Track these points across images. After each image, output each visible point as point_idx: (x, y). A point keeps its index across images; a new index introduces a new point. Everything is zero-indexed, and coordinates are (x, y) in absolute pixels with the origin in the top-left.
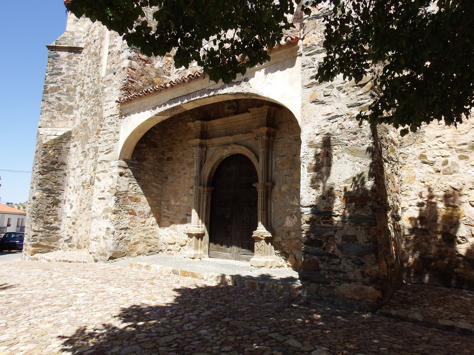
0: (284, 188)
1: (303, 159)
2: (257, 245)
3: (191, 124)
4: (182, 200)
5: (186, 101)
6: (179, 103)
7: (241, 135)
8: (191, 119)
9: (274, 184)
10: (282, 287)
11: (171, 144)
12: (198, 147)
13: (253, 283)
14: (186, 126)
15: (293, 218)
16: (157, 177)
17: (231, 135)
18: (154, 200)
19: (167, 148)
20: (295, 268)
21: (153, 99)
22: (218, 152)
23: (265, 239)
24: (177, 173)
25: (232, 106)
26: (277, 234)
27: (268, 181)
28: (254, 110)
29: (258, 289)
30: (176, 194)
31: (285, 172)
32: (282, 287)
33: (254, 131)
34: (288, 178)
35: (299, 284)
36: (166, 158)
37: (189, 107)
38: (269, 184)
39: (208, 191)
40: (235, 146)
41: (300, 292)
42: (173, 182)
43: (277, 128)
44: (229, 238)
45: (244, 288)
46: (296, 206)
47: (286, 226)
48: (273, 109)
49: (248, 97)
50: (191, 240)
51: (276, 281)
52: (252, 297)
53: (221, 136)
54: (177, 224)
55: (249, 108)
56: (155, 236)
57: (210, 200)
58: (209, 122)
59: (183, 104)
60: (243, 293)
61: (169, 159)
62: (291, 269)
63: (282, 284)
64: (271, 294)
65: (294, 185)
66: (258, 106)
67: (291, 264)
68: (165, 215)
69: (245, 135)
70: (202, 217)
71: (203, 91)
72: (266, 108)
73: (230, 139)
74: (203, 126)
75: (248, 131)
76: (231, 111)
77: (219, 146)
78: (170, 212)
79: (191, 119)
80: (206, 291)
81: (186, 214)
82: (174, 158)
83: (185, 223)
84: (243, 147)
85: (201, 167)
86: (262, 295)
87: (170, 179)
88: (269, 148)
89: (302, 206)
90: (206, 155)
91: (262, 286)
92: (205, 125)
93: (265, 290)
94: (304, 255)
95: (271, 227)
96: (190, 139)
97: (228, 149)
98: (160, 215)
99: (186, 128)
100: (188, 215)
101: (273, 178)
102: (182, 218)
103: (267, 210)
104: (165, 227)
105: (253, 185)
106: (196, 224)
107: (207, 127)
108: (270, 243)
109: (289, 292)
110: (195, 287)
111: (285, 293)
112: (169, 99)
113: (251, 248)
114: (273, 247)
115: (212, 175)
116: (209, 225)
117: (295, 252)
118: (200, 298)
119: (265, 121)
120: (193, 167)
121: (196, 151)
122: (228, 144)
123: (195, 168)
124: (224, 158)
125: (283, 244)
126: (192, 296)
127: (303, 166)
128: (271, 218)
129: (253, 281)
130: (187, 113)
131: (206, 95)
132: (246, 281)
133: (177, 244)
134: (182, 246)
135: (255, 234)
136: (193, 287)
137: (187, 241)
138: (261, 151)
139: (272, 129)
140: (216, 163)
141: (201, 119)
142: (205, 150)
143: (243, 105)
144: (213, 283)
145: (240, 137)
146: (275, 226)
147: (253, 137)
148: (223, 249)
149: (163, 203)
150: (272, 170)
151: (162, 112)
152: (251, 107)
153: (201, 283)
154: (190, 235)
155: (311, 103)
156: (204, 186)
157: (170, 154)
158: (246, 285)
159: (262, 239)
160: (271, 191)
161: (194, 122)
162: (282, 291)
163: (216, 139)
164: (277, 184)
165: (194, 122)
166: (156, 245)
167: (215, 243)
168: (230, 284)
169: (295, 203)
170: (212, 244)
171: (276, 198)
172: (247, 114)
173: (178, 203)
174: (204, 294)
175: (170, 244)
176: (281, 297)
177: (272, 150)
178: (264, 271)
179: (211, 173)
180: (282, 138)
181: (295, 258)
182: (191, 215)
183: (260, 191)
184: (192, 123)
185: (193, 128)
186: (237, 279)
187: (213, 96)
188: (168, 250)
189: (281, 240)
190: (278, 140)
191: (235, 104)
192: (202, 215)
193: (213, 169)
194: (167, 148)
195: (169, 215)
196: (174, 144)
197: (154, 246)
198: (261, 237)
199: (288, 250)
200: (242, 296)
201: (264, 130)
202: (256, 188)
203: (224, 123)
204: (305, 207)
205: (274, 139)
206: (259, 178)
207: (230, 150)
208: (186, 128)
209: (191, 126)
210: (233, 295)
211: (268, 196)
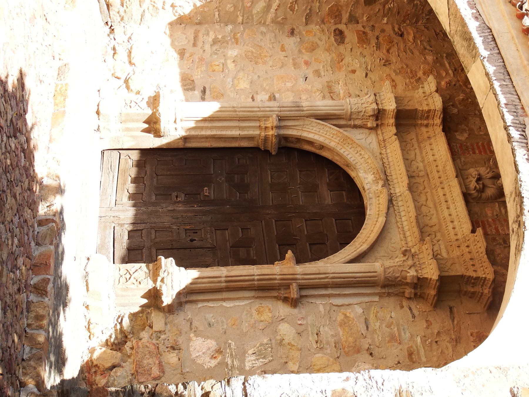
0: (286, 330)
1: (366, 376)
2: (140, 269)
3: (430, 84)
4: (241, 75)
5: (491, 69)
6: (484, 52)
7: (413, 214)
8: (443, 83)
9: (294, 303)
10: (41, 339)
11: (377, 38)
12: (374, 106)
13: (47, 266)
14: (426, 74)
15: (213, 357)
16: (292, 9)
17: (411, 188)
18: (235, 7)
19: (367, 30)
20: (89, 369)
22: (365, 157)
23: (155, 288)
24: (306, 58)
25: (484, 186)
26: (171, 317)
27: (302, 288)
28: (479, 242)
29: (35, 280)
30: (254, 58)
31: (327, 332)
32: (41, 339)
33: (424, 247)
34: (312, 338)
35: (51, 380)
36: (342, 27)
37: (476, 78)
38: (294, 293)
39: (266, 139)
40: (384, 200)
41: (31, 385)
42: (283, 49)
43: (438, 303)
44: (154, 197)
45: (33, 244)
46: (243, 362)
47: (190, 340)
48: (486, 291)
49: (513, 226)
50: (144, 104)
51: (55, 325)
52: (15, 267)
53: (408, 162)
54: (180, 66)
55: (484, 229)
56: (147, 15)
57: (245, 144)
58: (439, 130)
59: (482, 61)
60: (21, 244)
61: (340, 35)
62: (86, 359)
63: (48, 339)
64: (22, 313)
65: (296, 354)
66: (490, 253)
67: (98, 358)
68: (200, 35)
69: (414, 224)
70: (202, 128)
71: (520, 111)
72: (487, 272)
73: (400, 186)
74: (428, 114)
75: (424, 231)
76: (473, 184)
77: (382, 159)
78: (207, 47)
79: (443, 83)
80: (23, 151)
81: (205, 89)
82: (342, 48)
83: (183, 85)
84: (382, 220)
85: (325, 118)
86: (19, 290)
87: (291, 42)
88: (384, 286)
89: (246, 380)
90: (355, 127)
91: (40, 290)
92: (431, 122)
93: (33, 297)
94: (124, 393)
95: (187, 302)
96: (394, 86)
97: (376, 181)
98: (200, 23)
99: (420, 74)
100: (204, 91)
101: (310, 300)
102: (194, 78)
103: (228, 289)
104: (171, 36)
105: (290, 252)
106: (182, 118)
107: (427, 126)
108: (145, 301)
109: (30, 359)
110: (30, 124)
111: (27, 349)
112: (491, 26)
113: (132, 254)
114: (137, 309)
115: (307, 147)
116: (181, 145)
117: (128, 367)
118: (5, 138)
119: (453, 273)
120: (324, 97)
121: (366, 104)
122: (387, 182)
123: (324, 105)
124: (353, 174)
125: (145, 335)
126: (9, 117)
127: (347, 379)
128: (208, 301)
129: (52, 265)
130: (460, 71)
131: (509, 118)
132: (52, 247)
133: (129, 69)
134: (126, 81)
135: (168, 264)
136: (29, 118)
137: (138, 93)
138: (376, 267)
139: (433, 292)
140: (338, 154)
141: (445, 110)
142: (369, 125)
143: (489, 213)
144: (43, 167)
145: (406, 209)
146: (190, 311)
147: (410, 244)
148: (125, 184)
149: (230, 27)
150: (329, 296)
151: (457, 11)
152: (486, 234)
153: (39, 137)
154: (154, 101)
155: (511, 391)
156: (278, 127)
157: (351, 36)
158: (42, 249)
159: (155, 281)
160: (277, 298)
161: (437, 91)
162: (32, 340)
163: (399, 152)
164: (295, 311)
165: (437, 91)
166: (126, 19)
167: (140, 165)
168: (42, 209)
169: (250, 362)
170: (135, 156)
171: (259, 312)
172: (467, 226)
173: (231, 65)
174: (16, 148)
176: (16, 339)
177: (381, 295)
178: (76, 294)
179: (310, 143)
180: (414, 317)
181: (114, 367)
182: (203, 99)
183: (276, 270)
184: (434, 88)
185: (421, 90)
186: (55, 226)
187: (509, 136)
188: (114, 49)
189: (156, 328)
190: (406, 308)
191: (490, 192)
192: (207, 128)
193: (322, 147)
194: (367, 30)
195: (200, 44)
196: (378, 46)
197: (122, 13)
198: (159, 279)
199: (132, 348)
200: (16, 241)
201: (431, 272)
202: (283, 258)
203: (440, 168)
204: (245, 389)
205: (409, 299)
206: (307, 265)
207: (374, 188)
208: (420, 74)
209: (426, 85)
210: (16, 220)
211: (264, 289)
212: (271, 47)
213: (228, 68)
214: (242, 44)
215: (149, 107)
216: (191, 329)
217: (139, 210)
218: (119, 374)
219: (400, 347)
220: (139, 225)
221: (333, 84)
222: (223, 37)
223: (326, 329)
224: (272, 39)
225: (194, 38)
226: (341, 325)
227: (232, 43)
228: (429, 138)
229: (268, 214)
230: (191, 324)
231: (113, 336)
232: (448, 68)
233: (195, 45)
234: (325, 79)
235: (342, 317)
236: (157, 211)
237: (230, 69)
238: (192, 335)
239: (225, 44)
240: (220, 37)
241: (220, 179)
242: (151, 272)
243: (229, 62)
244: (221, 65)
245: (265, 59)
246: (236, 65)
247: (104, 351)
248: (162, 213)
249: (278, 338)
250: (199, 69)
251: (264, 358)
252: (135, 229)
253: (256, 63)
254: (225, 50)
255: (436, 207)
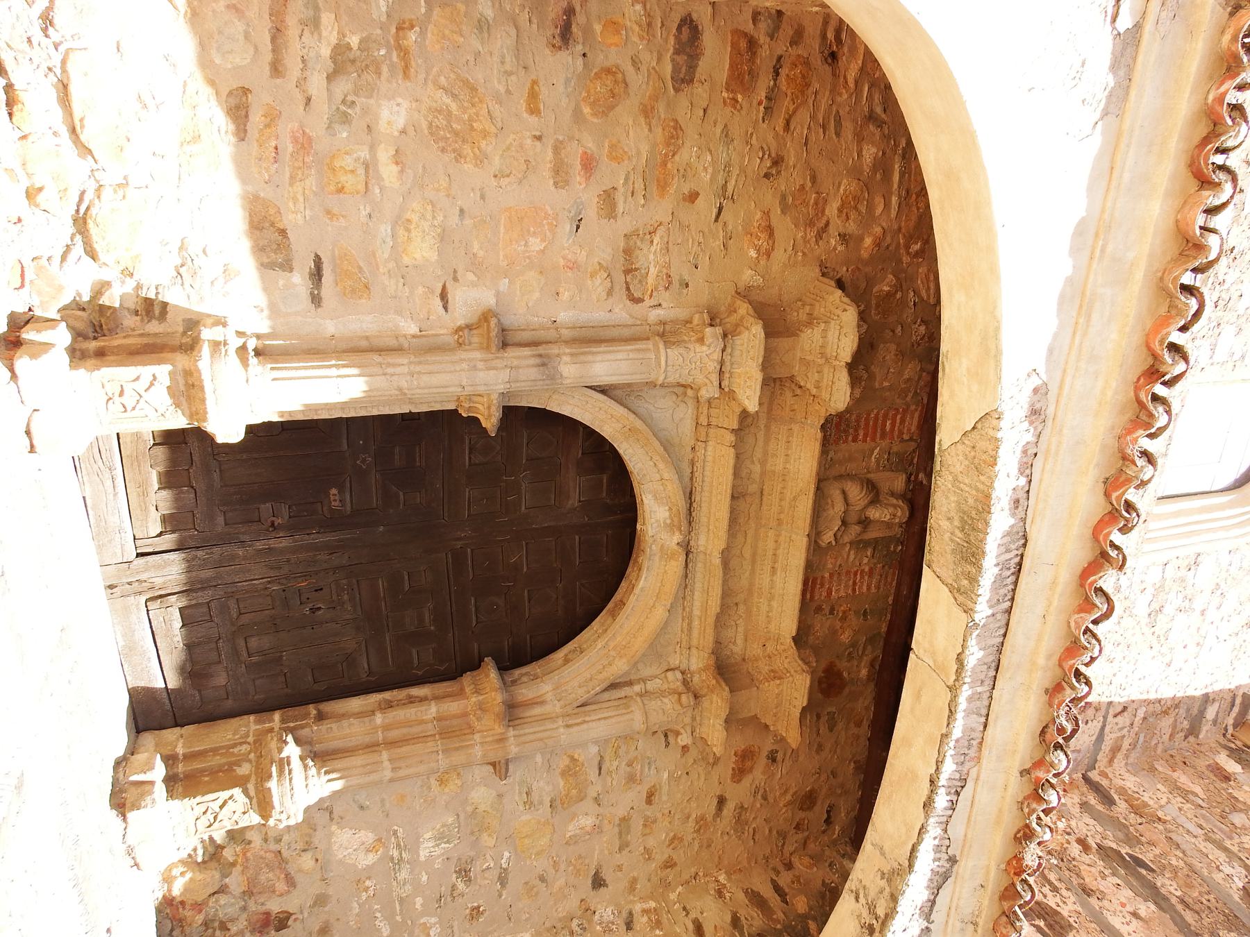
21: (1089, 422)
47: (331, 834)
78: (317, 84)
81: (318, 261)
97: (671, 527)
148: (144, 494)
173: (388, 171)
175: (64, 88)
212: (502, 89)
213: (380, 178)
214: (422, 76)
215: (177, 405)
216: (332, 819)
217: (193, 559)
218: (222, 902)
219: (639, 788)
220: (200, 594)
221: (639, 243)
222: (365, 44)
223: (542, 784)
224: (508, 59)
225: (274, 39)
226: (563, 774)
227: (392, 67)
228: (792, 420)
229: (459, 539)
230: (331, 813)
231: (200, 852)
232: (895, 186)
233: (277, 69)
234: (624, 224)
235: (567, 761)
236: (233, 557)
237: (387, 183)
238: (334, 828)
239: (369, 77)
240: (354, 41)
241: (364, 461)
242: (255, 800)
243: (384, 155)
244: (361, 171)
245: (483, 144)
246: (402, 171)
247: (191, 879)
248: (245, 558)
249: (469, 809)
250: (298, 187)
251: (448, 842)
252: (193, 602)
253: (459, 156)
254: (372, 101)
255: (754, 561)
